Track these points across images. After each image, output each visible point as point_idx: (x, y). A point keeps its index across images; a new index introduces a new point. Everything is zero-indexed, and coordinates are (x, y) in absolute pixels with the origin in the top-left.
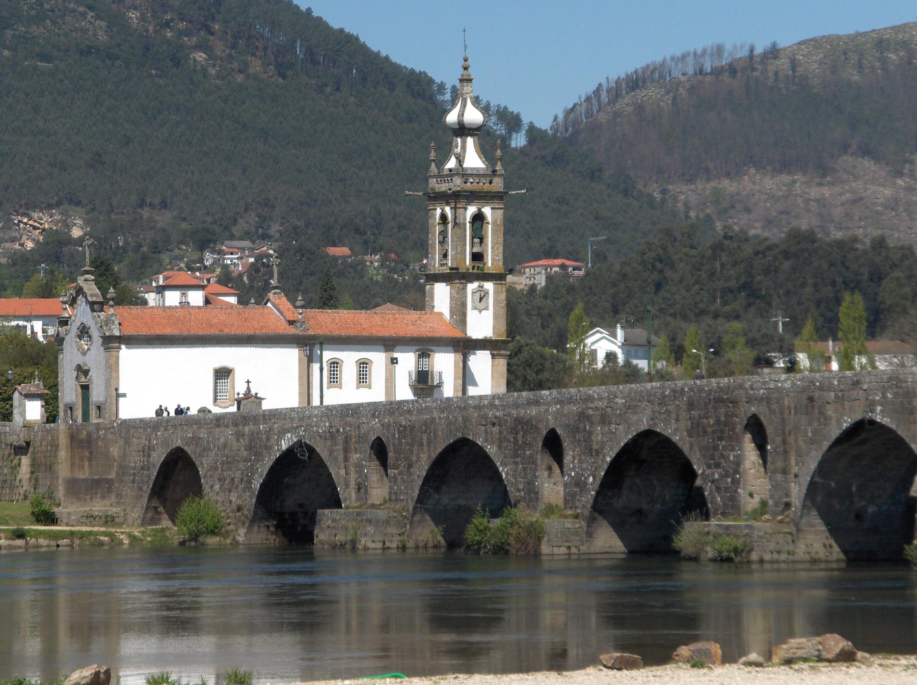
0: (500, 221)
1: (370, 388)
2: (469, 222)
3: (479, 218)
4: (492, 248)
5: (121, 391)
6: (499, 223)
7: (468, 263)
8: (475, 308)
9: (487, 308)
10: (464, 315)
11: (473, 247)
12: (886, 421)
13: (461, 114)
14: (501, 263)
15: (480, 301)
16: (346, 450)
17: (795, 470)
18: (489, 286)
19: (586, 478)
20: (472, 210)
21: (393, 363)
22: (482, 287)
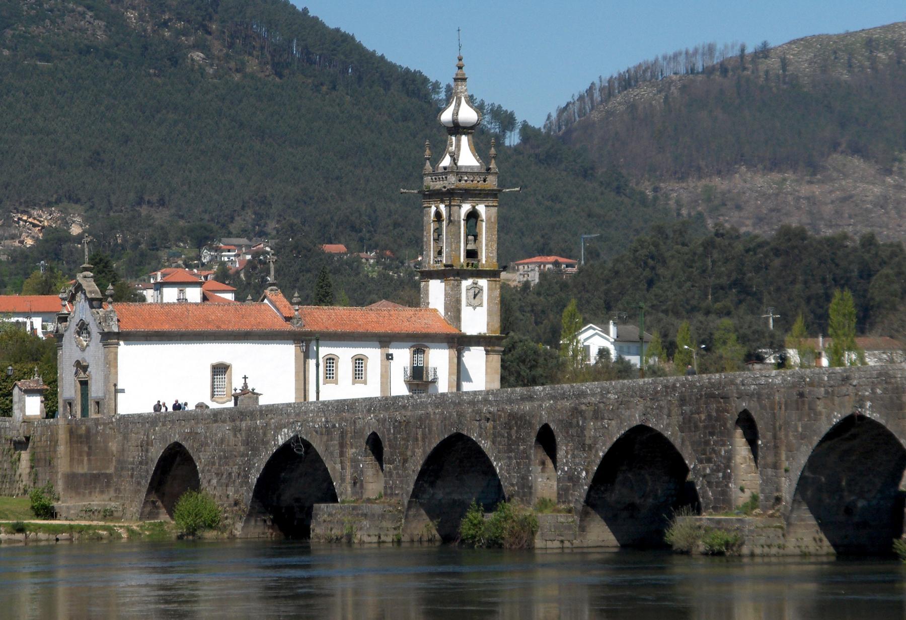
0: (495, 218)
1: (337, 384)
2: (464, 220)
3: (473, 216)
4: (487, 245)
5: (119, 387)
6: (493, 220)
7: (462, 260)
8: (469, 305)
9: (481, 305)
10: (458, 311)
11: (467, 244)
12: (876, 417)
13: (456, 113)
14: (495, 260)
15: (474, 298)
16: (342, 445)
17: (785, 464)
18: (483, 283)
19: (579, 473)
20: (466, 208)
21: (388, 359)
22: (476, 284)
